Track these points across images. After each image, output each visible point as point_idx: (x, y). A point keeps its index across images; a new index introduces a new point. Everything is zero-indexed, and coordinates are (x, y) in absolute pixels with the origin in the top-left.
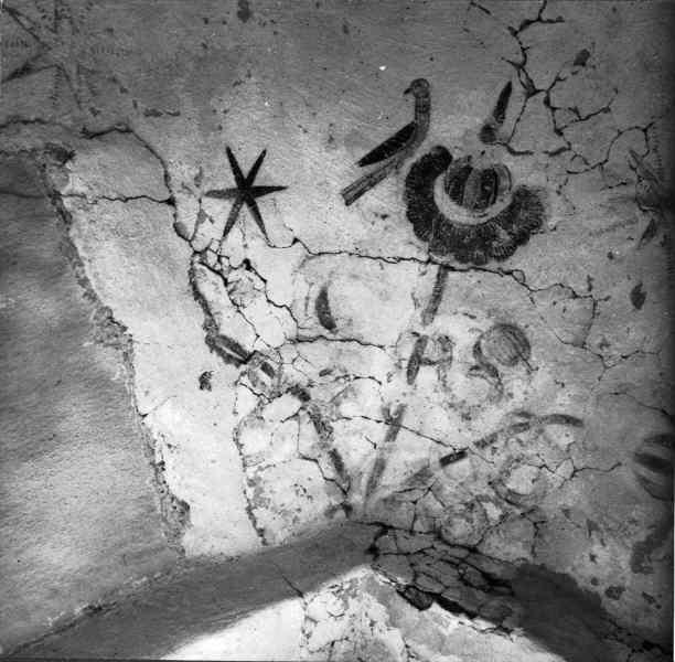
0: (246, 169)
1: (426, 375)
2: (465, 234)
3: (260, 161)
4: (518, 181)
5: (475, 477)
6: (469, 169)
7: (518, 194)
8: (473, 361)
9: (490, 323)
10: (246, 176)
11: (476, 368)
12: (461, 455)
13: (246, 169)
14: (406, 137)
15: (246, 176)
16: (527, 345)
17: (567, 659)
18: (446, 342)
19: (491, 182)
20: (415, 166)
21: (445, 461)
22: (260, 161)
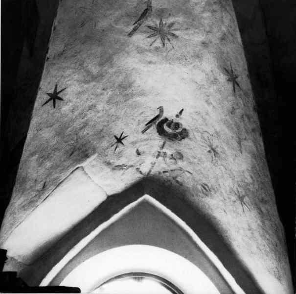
0: (58, 90)
1: (160, 158)
2: (170, 134)
3: (46, 103)
4: (183, 127)
5: (170, 176)
6: (172, 122)
7: (183, 129)
8: (171, 157)
9: (175, 151)
10: (57, 92)
11: (171, 158)
12: (167, 172)
13: (58, 90)
14: (158, 117)
15: (57, 92)
16: (183, 157)
17: (221, 293)
18: (165, 153)
19: (177, 125)
20: (159, 123)
21: (164, 172)
22: (46, 103)
